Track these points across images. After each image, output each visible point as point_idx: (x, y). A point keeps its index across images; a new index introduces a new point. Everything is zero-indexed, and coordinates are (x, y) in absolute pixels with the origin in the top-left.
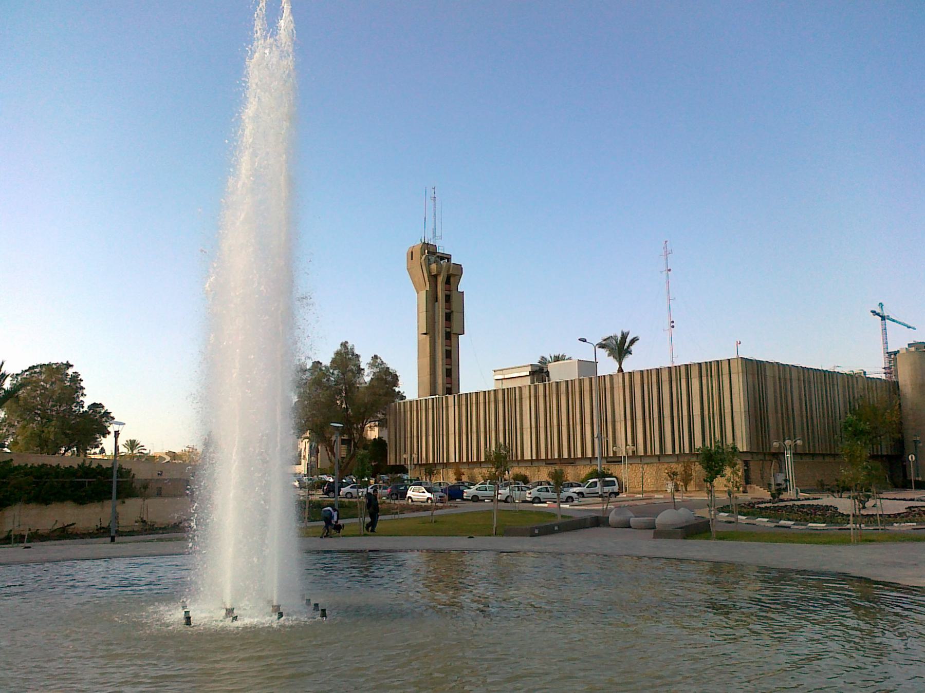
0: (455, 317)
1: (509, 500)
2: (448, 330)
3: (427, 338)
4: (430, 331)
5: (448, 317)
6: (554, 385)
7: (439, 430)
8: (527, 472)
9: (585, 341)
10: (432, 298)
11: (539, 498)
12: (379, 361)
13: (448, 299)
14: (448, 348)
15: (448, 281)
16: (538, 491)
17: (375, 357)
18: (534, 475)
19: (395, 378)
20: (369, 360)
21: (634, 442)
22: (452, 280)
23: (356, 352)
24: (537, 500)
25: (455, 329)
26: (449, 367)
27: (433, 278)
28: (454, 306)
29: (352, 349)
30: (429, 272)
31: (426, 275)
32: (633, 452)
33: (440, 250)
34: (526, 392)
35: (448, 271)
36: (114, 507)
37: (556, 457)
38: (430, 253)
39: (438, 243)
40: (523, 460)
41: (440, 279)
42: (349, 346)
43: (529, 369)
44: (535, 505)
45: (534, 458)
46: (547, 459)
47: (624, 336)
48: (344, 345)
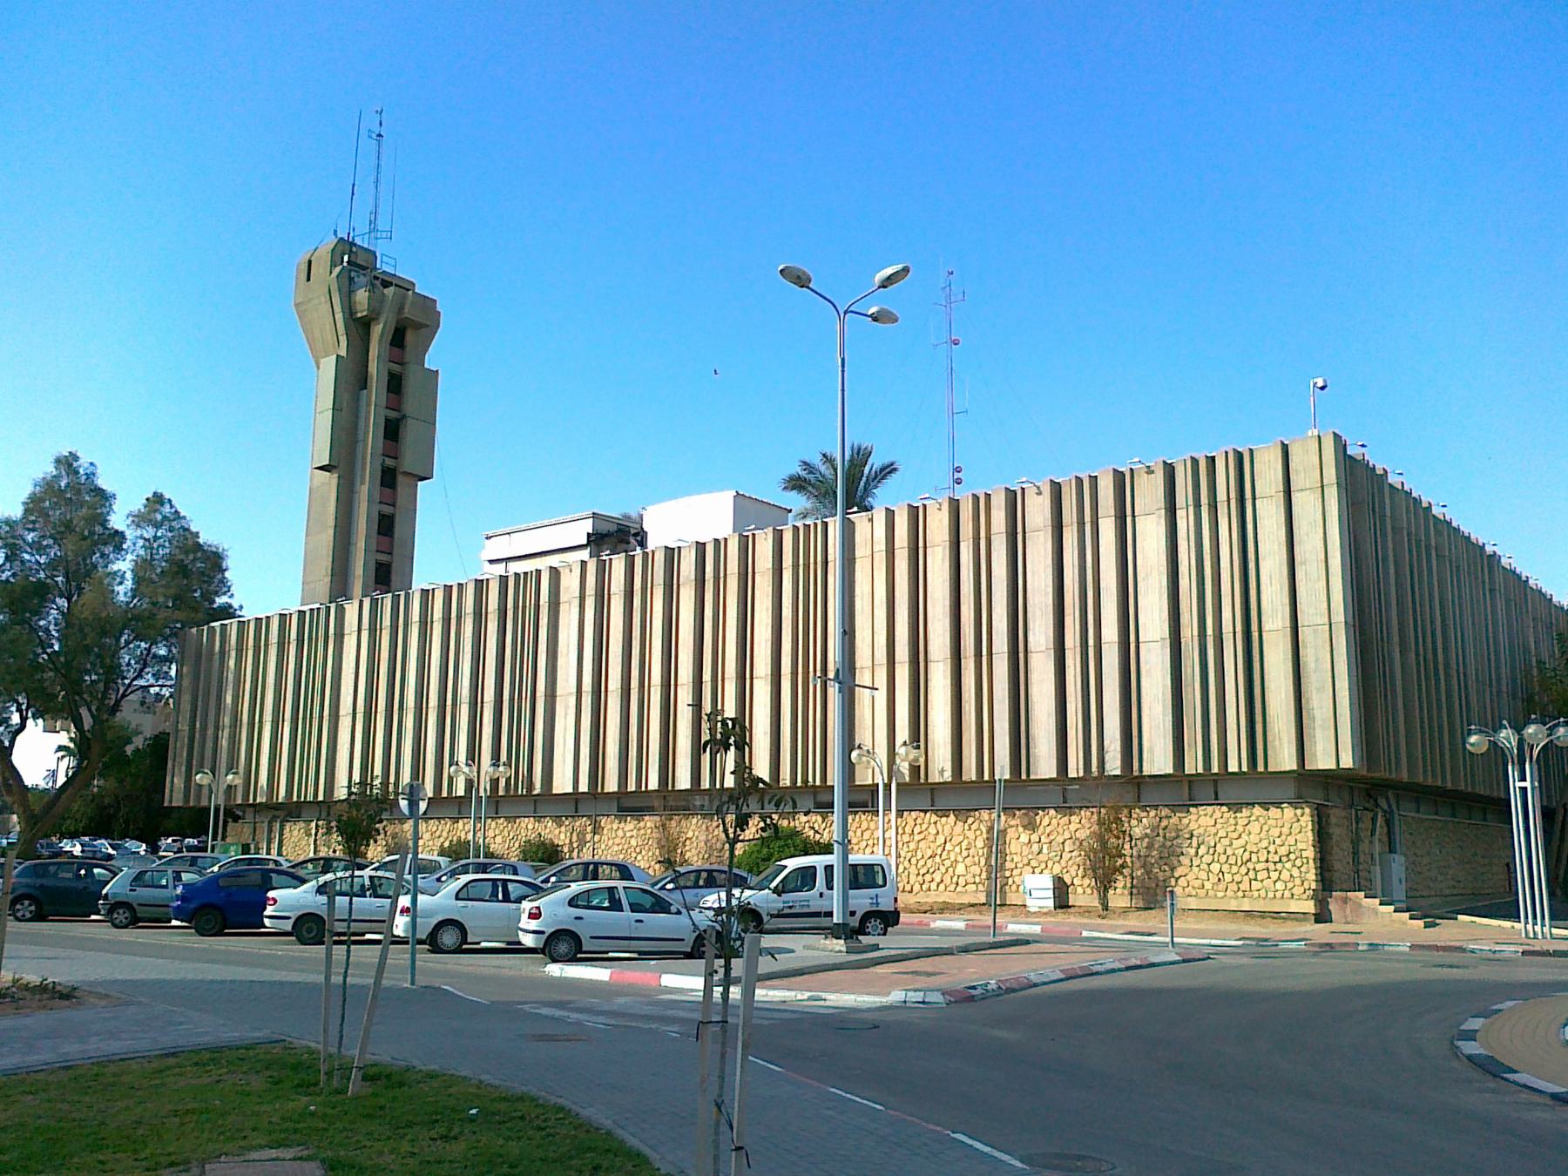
0: (410, 432)
1: (449, 938)
2: (390, 462)
3: (331, 480)
4: (341, 462)
5: (392, 431)
6: (660, 558)
7: (310, 705)
8: (558, 834)
9: (801, 280)
10: (352, 379)
11: (573, 937)
12: (167, 509)
13: (395, 384)
14: (387, 510)
15: (398, 338)
16: (572, 902)
17: (158, 500)
18: (582, 843)
19: (214, 562)
20: (138, 504)
21: (918, 733)
22: (410, 337)
23: (102, 482)
24: (563, 944)
25: (408, 463)
26: (384, 558)
27: (359, 328)
28: (410, 405)
29: (90, 476)
30: (349, 310)
31: (339, 316)
32: (915, 769)
33: (384, 266)
34: (570, 583)
35: (401, 309)
36: (997, 844)
37: (653, 784)
38: (354, 263)
39: (380, 248)
40: (548, 795)
41: (377, 330)
42: (83, 464)
43: (587, 526)
44: (555, 970)
45: (584, 787)
46: (622, 793)
47: (860, 457)
48: (67, 463)
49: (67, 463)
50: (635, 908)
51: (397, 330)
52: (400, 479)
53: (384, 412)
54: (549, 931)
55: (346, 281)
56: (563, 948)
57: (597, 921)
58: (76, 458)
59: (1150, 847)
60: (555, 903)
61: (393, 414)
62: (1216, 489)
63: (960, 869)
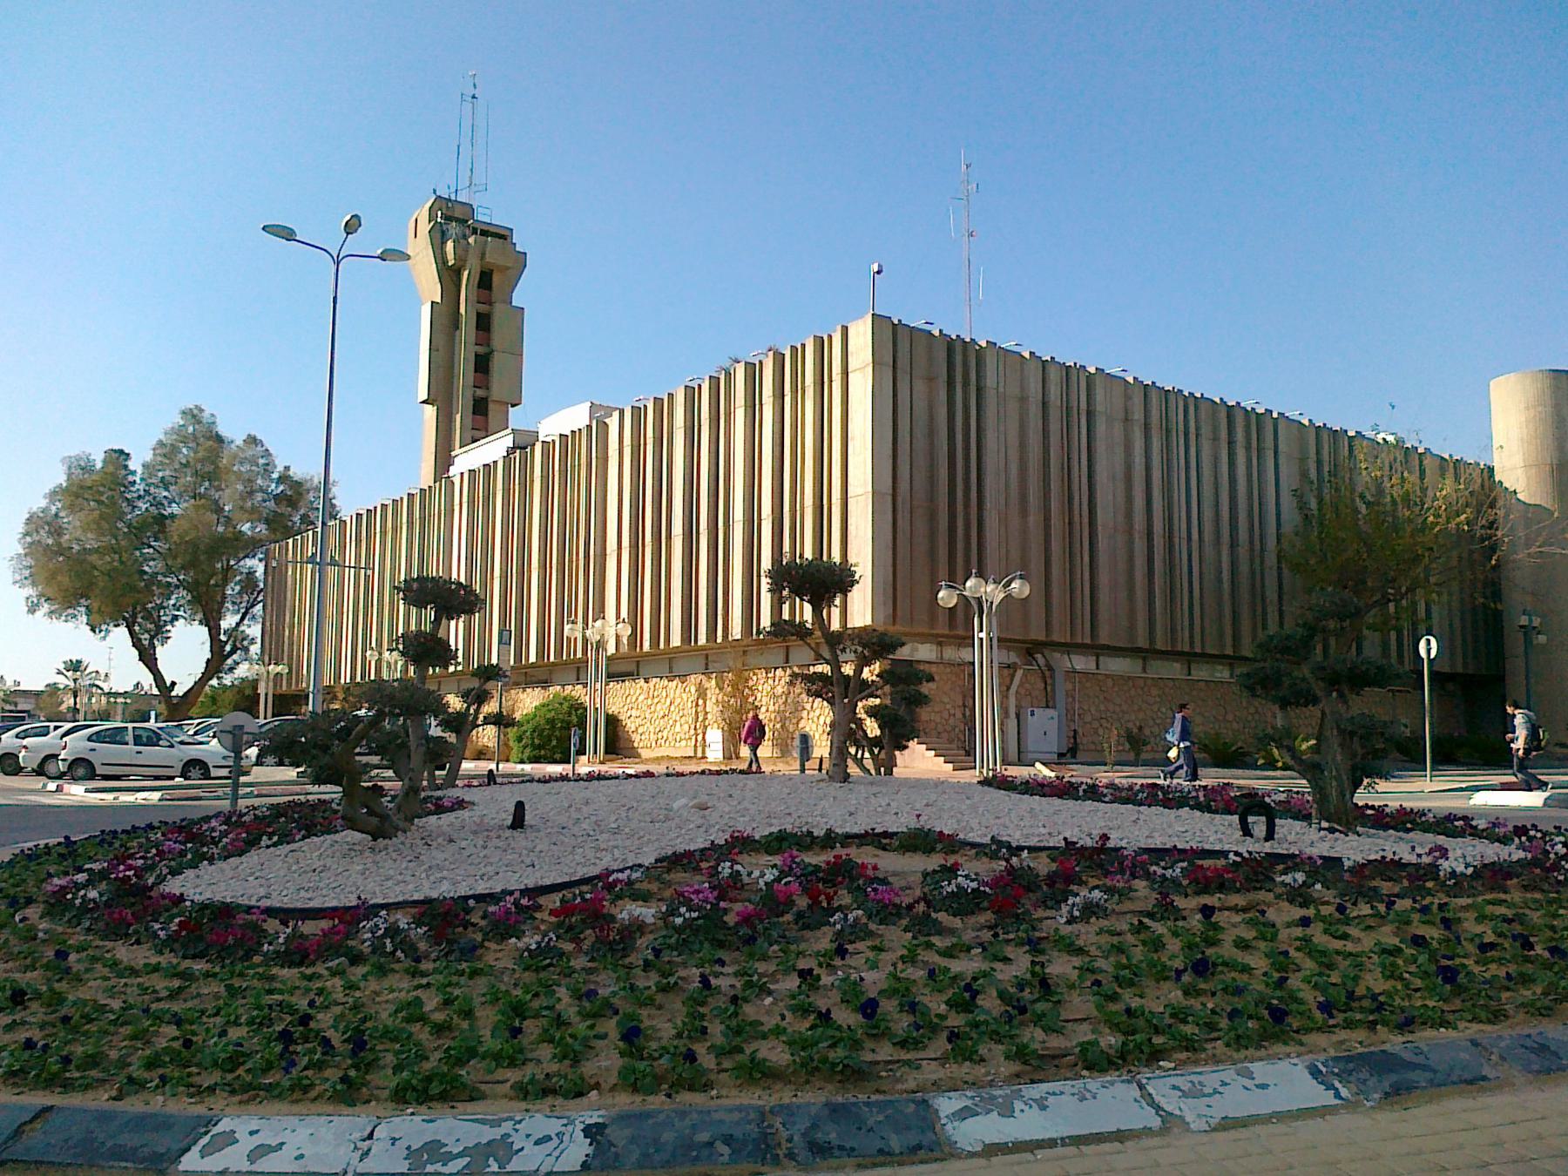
0: (497, 362)
5: (482, 365)
9: (288, 234)
13: (483, 323)
15: (485, 281)
22: (496, 279)
25: (497, 391)
28: (498, 338)
49: (193, 415)
50: (138, 741)
51: (482, 273)
52: (491, 406)
53: (474, 349)
54: (71, 758)
55: (439, 235)
56: (81, 771)
57: (105, 753)
58: (202, 411)
59: (785, 703)
60: (80, 739)
61: (481, 350)
62: (802, 371)
63: (678, 728)
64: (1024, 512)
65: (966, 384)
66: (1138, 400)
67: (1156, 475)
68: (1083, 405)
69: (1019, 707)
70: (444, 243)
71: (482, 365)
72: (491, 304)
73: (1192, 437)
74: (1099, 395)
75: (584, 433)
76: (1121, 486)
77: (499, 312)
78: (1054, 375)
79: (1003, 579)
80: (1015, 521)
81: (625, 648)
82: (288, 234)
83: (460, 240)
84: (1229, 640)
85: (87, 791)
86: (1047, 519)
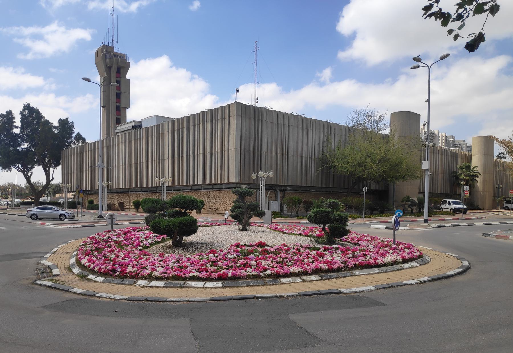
5: (118, 96)
9: (88, 80)
22: (122, 71)
25: (123, 104)
64: (271, 153)
65: (258, 120)
66: (300, 122)
67: (304, 141)
68: (287, 124)
69: (269, 201)
70: (106, 59)
71: (118, 96)
72: (120, 78)
73: (314, 131)
74: (291, 121)
75: (158, 126)
76: (296, 144)
77: (122, 80)
78: (280, 116)
79: (267, 171)
80: (269, 155)
81: (170, 184)
82: (88, 80)
83: (111, 58)
84: (320, 183)
85: (507, 238)
86: (277, 154)
